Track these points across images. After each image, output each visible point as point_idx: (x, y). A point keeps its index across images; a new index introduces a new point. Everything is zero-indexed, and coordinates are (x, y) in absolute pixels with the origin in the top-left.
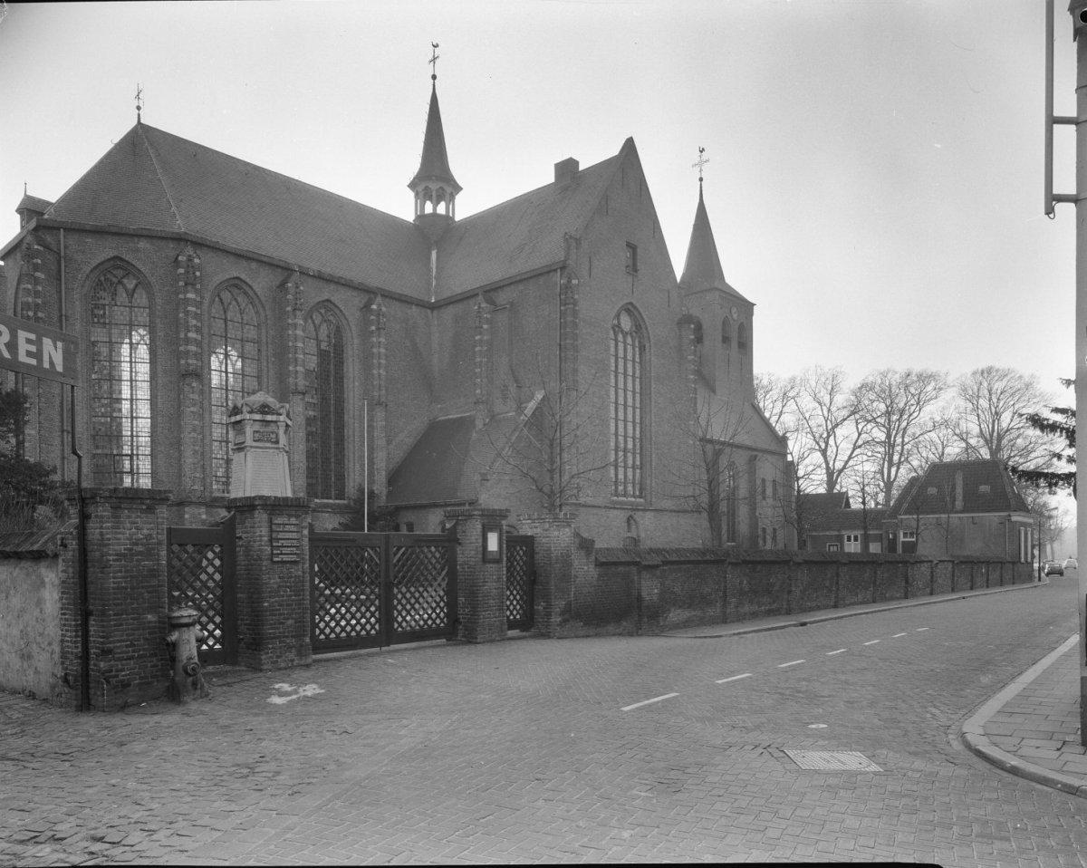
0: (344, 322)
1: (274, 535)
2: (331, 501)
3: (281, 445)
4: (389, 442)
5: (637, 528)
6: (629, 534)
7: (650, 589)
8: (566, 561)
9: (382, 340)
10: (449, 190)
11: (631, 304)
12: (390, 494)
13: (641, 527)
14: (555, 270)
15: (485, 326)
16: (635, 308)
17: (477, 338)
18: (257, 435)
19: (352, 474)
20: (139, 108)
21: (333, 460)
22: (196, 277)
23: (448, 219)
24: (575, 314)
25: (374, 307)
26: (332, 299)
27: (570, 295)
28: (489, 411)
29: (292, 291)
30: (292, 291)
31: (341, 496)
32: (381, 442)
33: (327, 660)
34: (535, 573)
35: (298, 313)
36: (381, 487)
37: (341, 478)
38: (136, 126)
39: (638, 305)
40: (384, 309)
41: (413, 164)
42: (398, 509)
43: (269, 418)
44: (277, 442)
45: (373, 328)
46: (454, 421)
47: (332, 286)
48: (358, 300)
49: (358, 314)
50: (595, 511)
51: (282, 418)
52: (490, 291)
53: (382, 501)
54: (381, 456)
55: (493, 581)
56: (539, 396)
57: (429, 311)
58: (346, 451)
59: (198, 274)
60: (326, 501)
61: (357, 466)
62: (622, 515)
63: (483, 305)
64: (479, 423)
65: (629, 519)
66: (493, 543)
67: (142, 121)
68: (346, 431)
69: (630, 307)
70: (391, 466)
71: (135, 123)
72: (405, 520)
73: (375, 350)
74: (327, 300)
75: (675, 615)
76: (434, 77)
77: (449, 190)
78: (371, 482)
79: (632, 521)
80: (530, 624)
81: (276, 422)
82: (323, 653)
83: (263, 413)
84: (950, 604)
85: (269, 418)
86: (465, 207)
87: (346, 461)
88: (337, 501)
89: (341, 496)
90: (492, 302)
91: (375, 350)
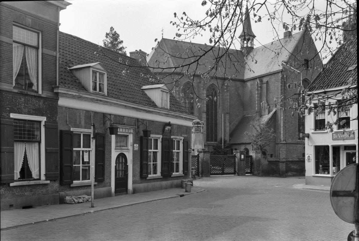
2: (213, 142)
3: (201, 132)
4: (230, 124)
7: (282, 167)
10: (251, 38)
12: (230, 140)
14: (280, 72)
18: (196, 130)
19: (219, 134)
20: (162, 34)
21: (214, 130)
22: (179, 84)
26: (214, 83)
28: (260, 114)
31: (216, 140)
32: (228, 124)
33: (215, 176)
35: (205, 90)
36: (227, 138)
37: (216, 135)
38: (162, 40)
39: (308, 79)
40: (229, 85)
42: (232, 144)
43: (199, 125)
44: (201, 131)
50: (292, 145)
51: (202, 125)
53: (228, 142)
54: (228, 129)
58: (218, 127)
59: (179, 83)
60: (212, 142)
61: (221, 131)
66: (243, 157)
68: (218, 121)
69: (306, 79)
70: (231, 131)
71: (162, 38)
72: (234, 148)
74: (213, 84)
75: (289, 174)
77: (251, 38)
78: (225, 136)
81: (200, 126)
82: (110, 165)
83: (198, 124)
84: (320, 178)
85: (199, 125)
87: (217, 130)
88: (215, 142)
89: (216, 140)
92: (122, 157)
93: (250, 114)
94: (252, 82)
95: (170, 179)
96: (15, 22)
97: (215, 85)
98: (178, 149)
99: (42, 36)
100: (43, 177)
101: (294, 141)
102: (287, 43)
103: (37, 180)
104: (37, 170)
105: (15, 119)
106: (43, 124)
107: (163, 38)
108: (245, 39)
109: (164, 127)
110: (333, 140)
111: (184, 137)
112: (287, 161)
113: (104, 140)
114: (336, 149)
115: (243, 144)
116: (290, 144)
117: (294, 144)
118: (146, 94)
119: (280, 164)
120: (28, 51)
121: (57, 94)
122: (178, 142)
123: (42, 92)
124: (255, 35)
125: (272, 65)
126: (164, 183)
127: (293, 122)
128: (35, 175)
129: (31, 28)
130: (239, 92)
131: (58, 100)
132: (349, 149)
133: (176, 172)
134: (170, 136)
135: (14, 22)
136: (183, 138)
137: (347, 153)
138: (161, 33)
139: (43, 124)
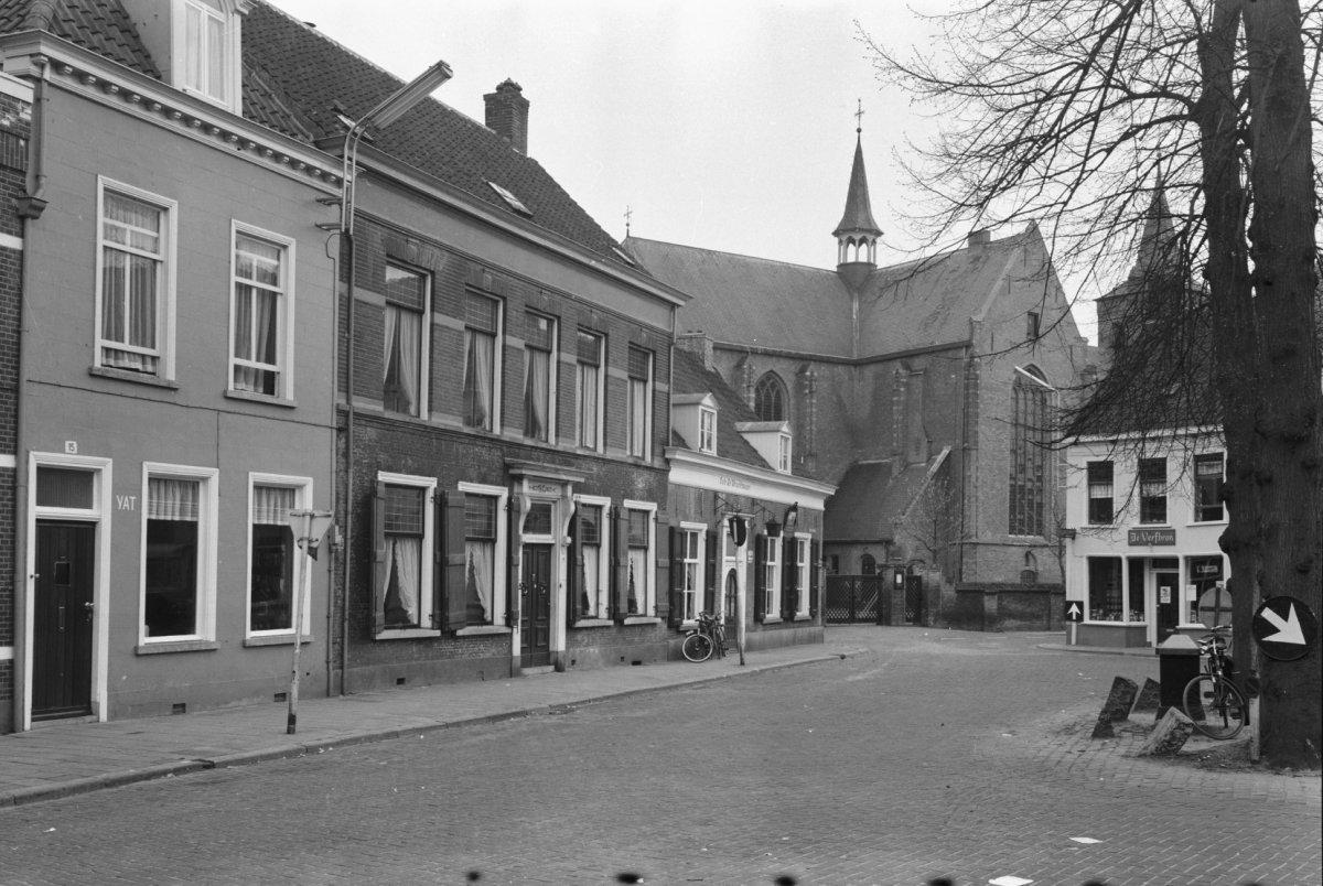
0: (782, 386)
1: (10, 588)
5: (1036, 561)
6: (1027, 568)
7: (991, 604)
8: (937, 589)
9: (814, 401)
11: (1033, 366)
13: (1039, 561)
15: (902, 389)
16: (1036, 368)
17: (895, 399)
20: (628, 225)
23: (870, 265)
24: (976, 385)
25: (808, 373)
27: (972, 371)
29: (747, 372)
30: (747, 372)
34: (920, 594)
41: (838, 214)
45: (807, 391)
46: (873, 465)
47: (774, 359)
48: (794, 367)
49: (794, 378)
50: (993, 548)
52: (906, 356)
55: (899, 599)
56: (946, 451)
57: (853, 369)
62: (1021, 552)
63: (901, 371)
64: (895, 472)
65: (1027, 555)
66: (899, 579)
67: (631, 235)
73: (808, 410)
74: (771, 371)
75: (1008, 623)
76: (859, 131)
77: (870, 237)
79: (1030, 557)
80: (918, 620)
86: (888, 255)
90: (907, 367)
91: (808, 410)
92: (733, 575)
93: (873, 457)
94: (879, 368)
95: (792, 625)
96: (470, 286)
97: (778, 375)
98: (694, 555)
99: (654, 361)
100: (651, 612)
101: (998, 538)
102: (979, 265)
103: (642, 616)
104: (643, 598)
105: (468, 495)
106: (430, 494)
107: (628, 236)
108: (850, 240)
109: (787, 515)
110: (1131, 544)
111: (813, 534)
112: (1001, 592)
113: (1060, 563)
114: (1137, 565)
115: (861, 543)
116: (988, 544)
117: (997, 545)
118: (746, 442)
119: (986, 598)
120: (632, 391)
121: (667, 461)
122: (694, 535)
123: (653, 459)
124: (881, 227)
125: (937, 324)
126: (786, 633)
127: (998, 485)
128: (640, 610)
129: (491, 293)
130: (842, 393)
131: (669, 471)
132: (1161, 567)
133: (1177, 567)
134: (793, 533)
135: (467, 284)
136: (809, 536)
137: (1158, 574)
138: (625, 220)
139: (430, 494)
